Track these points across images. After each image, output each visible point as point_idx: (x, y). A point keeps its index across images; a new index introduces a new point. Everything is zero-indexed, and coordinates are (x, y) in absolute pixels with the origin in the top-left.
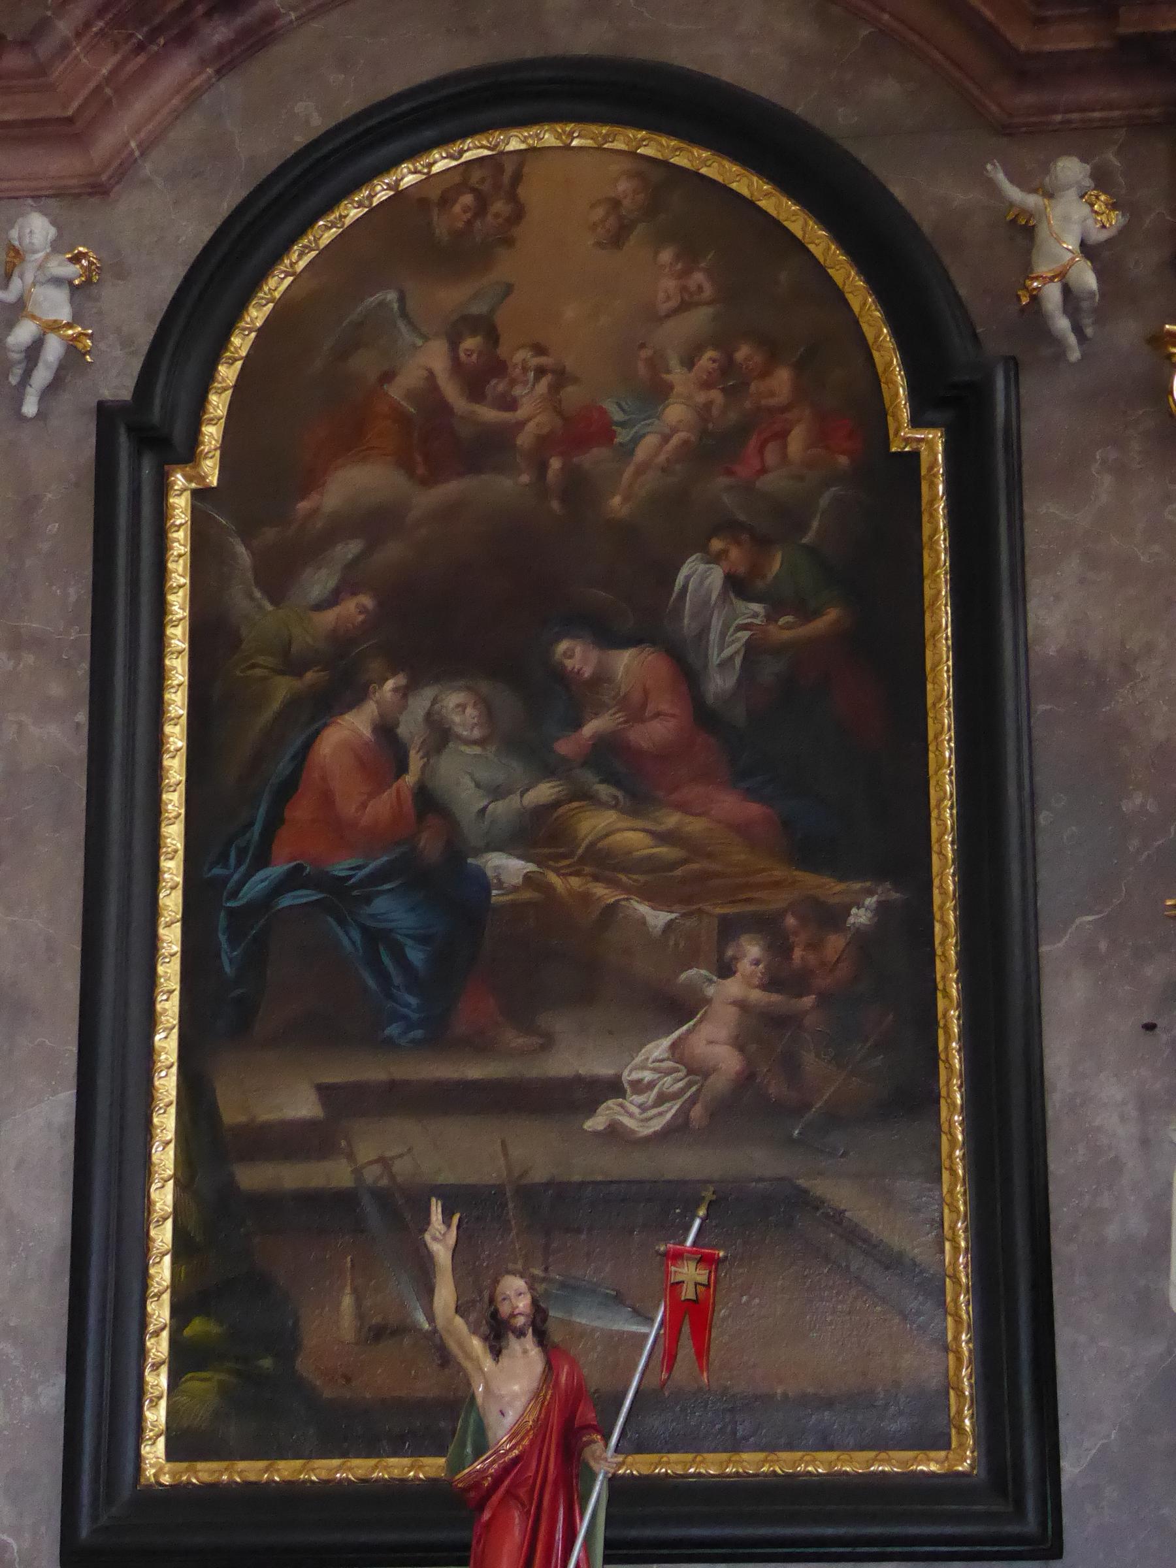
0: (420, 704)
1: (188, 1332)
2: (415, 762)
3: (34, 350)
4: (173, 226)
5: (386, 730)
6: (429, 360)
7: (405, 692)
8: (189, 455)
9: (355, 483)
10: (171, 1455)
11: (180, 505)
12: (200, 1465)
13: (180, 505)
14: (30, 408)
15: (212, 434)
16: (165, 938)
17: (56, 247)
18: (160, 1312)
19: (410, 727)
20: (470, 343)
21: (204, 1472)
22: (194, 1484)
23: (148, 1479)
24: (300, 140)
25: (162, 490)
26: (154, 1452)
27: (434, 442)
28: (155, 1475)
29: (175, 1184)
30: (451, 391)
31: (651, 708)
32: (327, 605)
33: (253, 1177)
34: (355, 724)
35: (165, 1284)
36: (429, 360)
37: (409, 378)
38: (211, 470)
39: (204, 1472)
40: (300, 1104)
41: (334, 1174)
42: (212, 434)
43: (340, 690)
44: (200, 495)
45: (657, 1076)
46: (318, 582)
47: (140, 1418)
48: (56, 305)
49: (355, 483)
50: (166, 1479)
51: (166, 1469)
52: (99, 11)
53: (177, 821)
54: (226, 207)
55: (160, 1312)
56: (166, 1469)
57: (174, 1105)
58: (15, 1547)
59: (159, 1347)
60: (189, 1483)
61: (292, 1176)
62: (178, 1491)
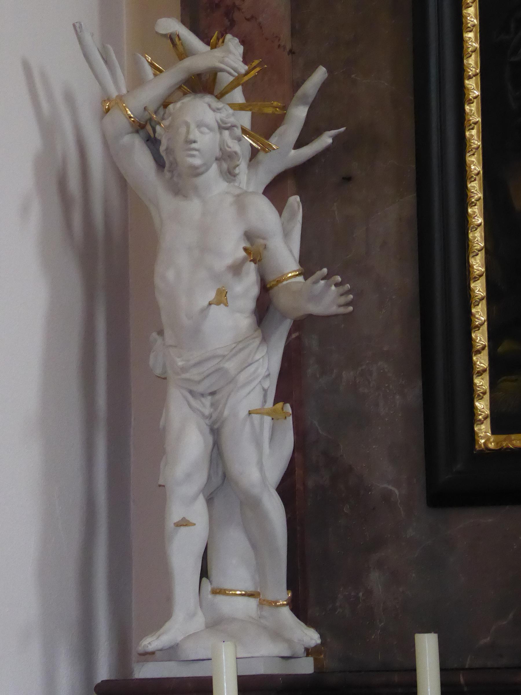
1: (500, 349)
10: (495, 431)
12: (513, 436)
16: (469, 86)
18: (480, 338)
22: (511, 449)
23: (480, 446)
26: (484, 432)
28: (485, 443)
29: (486, 253)
31: (228, 97)
35: (483, 319)
47: (472, 407)
50: (492, 446)
51: (492, 440)
53: (484, 374)
55: (480, 338)
56: (492, 440)
57: (485, 299)
58: (397, 492)
59: (481, 361)
60: (508, 448)
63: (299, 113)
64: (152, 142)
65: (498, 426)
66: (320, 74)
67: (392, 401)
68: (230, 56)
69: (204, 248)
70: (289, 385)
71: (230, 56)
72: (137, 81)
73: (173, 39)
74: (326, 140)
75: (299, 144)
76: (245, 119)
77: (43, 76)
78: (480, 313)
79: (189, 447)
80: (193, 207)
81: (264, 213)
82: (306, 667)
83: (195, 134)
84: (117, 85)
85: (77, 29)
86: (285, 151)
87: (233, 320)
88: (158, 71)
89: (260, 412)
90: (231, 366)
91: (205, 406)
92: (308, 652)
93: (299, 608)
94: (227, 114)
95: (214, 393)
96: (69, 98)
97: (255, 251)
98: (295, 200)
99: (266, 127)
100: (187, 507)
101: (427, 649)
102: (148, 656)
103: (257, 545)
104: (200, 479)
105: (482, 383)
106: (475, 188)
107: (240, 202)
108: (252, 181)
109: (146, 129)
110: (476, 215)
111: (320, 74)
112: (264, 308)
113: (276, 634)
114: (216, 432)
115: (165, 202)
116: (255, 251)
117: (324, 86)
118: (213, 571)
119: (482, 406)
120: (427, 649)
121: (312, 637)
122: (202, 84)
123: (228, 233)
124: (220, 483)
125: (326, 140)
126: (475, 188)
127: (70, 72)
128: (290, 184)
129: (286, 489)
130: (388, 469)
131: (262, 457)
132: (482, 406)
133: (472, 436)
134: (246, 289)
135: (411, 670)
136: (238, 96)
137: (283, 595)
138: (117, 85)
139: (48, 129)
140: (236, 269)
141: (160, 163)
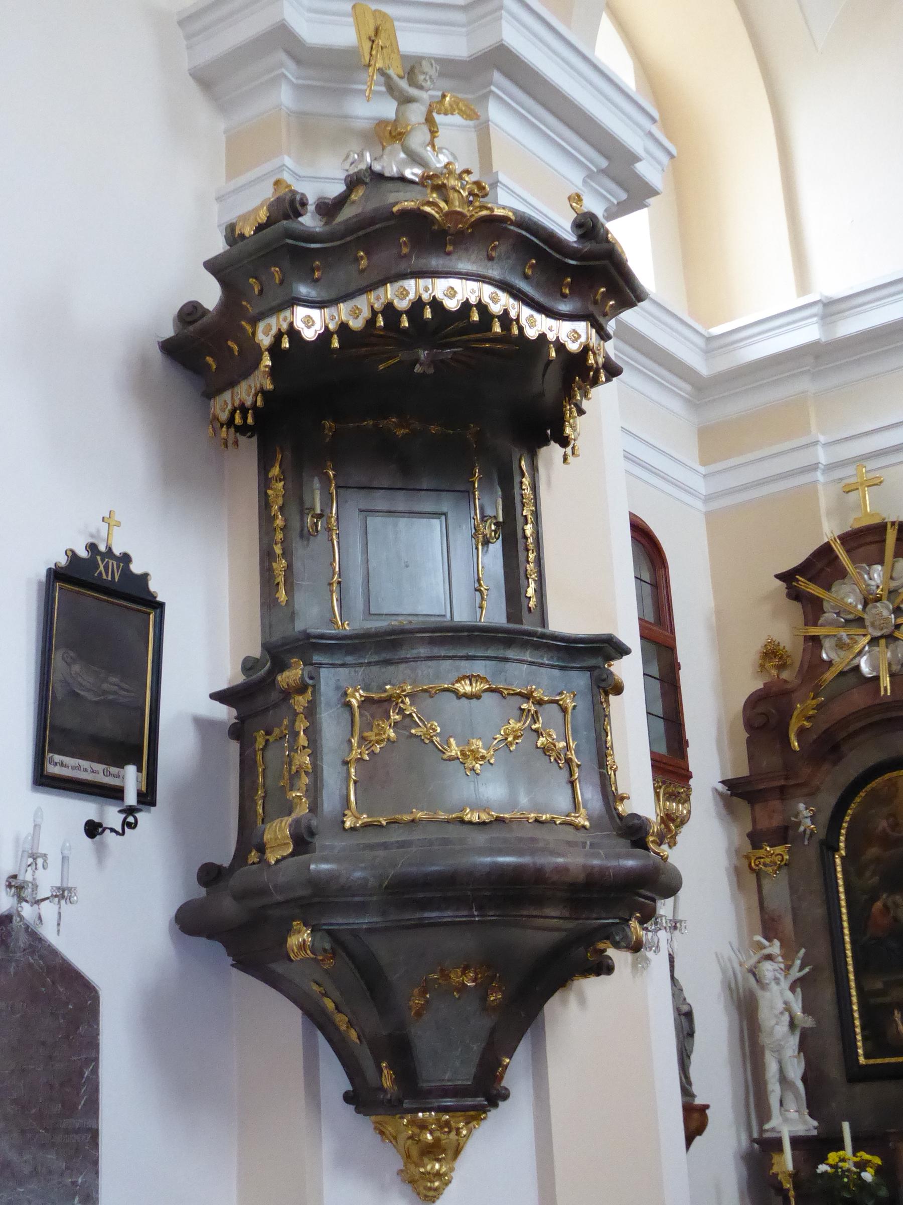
0: (890, 900)
2: (892, 912)
3: (805, 831)
4: (829, 800)
5: (885, 906)
6: (883, 824)
7: (888, 897)
8: (837, 849)
9: (873, 851)
11: (838, 861)
13: (838, 861)
14: (806, 843)
15: (842, 845)
17: (806, 809)
19: (890, 904)
20: (891, 820)
21: (871, 1062)
24: (852, 779)
25: (834, 858)
26: (862, 1060)
27: (886, 842)
30: (888, 830)
32: (871, 880)
33: (872, 1001)
34: (879, 905)
36: (883, 824)
37: (880, 828)
38: (843, 853)
39: (871, 1062)
40: (879, 985)
41: (887, 999)
42: (842, 845)
43: (874, 899)
44: (842, 858)
45: (294, 768)
46: (868, 874)
48: (808, 822)
49: (873, 851)
52: (673, 958)
54: (839, 794)
55: (858, 1030)
61: (880, 1000)
62: (866, 1066)
63: (798, 962)
64: (754, 975)
65: (866, 1057)
66: (803, 951)
67: (834, 1049)
68: (775, 948)
69: (772, 1008)
70: (803, 1046)
71: (775, 948)
72: (750, 957)
73: (759, 942)
74: (807, 970)
75: (800, 970)
76: (782, 966)
77: (722, 957)
78: (857, 1023)
79: (772, 1068)
80: (767, 994)
81: (789, 995)
82: (815, 1133)
83: (766, 973)
84: (743, 958)
85: (730, 944)
86: (795, 974)
87: (782, 1028)
88: (755, 954)
89: (794, 1057)
90: (782, 1043)
91: (776, 1055)
92: (815, 1128)
93: (811, 1115)
94: (776, 966)
95: (778, 1050)
96: (730, 960)
97: (788, 1008)
98: (799, 990)
99: (788, 968)
100: (774, 1090)
101: (846, 1127)
102: (767, 1131)
103: (797, 1097)
104: (777, 1076)
105: (860, 1044)
106: (853, 984)
107: (782, 993)
108: (785, 984)
109: (753, 972)
110: (853, 992)
111: (803, 951)
112: (792, 1025)
113: (805, 1122)
114: (780, 1063)
115: (759, 993)
116: (788, 1008)
117: (805, 954)
118: (784, 1104)
119: (860, 1051)
120: (846, 1127)
121: (815, 1123)
122: (769, 957)
123: (780, 1001)
124: (783, 1080)
125: (807, 970)
126: (853, 984)
127: (727, 952)
128: (798, 984)
129: (804, 1079)
130: (834, 1071)
131: (796, 1071)
132: (860, 1051)
133: (858, 1061)
134: (786, 1018)
135: (841, 1132)
136: (780, 959)
137: (806, 1111)
138: (743, 958)
139: (724, 971)
140: (782, 1013)
141: (757, 981)
